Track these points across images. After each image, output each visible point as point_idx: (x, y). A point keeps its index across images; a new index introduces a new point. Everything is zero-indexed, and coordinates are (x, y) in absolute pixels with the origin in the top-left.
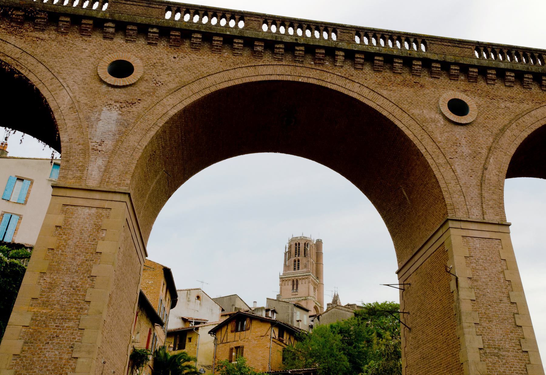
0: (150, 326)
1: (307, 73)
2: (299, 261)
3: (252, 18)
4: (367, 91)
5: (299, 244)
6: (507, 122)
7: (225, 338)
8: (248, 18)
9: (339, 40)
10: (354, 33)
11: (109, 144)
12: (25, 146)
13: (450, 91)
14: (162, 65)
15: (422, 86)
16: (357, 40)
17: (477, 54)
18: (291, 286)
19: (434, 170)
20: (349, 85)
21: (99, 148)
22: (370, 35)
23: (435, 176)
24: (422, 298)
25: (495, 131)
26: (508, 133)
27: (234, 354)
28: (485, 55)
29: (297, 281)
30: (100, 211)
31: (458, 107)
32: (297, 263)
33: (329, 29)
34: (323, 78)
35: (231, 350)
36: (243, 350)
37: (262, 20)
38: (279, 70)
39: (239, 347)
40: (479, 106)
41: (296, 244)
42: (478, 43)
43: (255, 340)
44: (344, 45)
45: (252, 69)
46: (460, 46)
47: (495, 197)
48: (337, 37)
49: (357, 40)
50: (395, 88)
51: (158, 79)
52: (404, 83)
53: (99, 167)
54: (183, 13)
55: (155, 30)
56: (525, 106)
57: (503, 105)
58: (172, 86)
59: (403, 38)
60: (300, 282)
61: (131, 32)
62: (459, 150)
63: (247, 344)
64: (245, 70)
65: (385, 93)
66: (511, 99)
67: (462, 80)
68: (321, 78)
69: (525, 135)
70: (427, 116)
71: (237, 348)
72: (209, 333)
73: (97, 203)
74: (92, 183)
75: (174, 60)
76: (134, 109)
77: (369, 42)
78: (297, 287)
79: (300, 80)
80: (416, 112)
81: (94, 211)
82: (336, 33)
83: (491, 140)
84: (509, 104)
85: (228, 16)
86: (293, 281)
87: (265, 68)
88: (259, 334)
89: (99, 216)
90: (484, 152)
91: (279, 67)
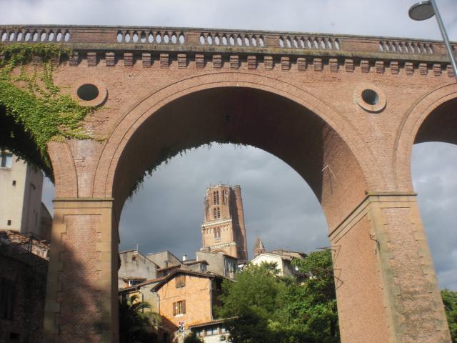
0: (145, 301)
1: (243, 78)
2: (219, 209)
3: (190, 33)
4: (295, 89)
5: (218, 192)
6: (409, 106)
7: (167, 295)
8: (187, 33)
9: (267, 45)
10: (278, 37)
11: (89, 159)
12: (18, 168)
13: (362, 81)
14: (121, 84)
15: (340, 80)
16: (281, 43)
17: (381, 47)
18: (214, 234)
19: (355, 154)
20: (279, 86)
21: (83, 164)
22: (292, 38)
23: (356, 159)
24: (352, 257)
25: (401, 115)
26: (411, 116)
27: (177, 308)
28: (388, 48)
29: (218, 228)
30: (93, 217)
31: (369, 97)
32: (217, 211)
33: (257, 36)
34: (256, 81)
35: (174, 304)
36: (185, 304)
37: (199, 34)
38: (220, 78)
39: (181, 301)
40: (386, 94)
41: (215, 193)
42: (381, 38)
43: (195, 294)
44: (270, 50)
45: (196, 79)
46: (367, 41)
47: (404, 172)
48: (264, 43)
49: (281, 43)
50: (317, 84)
51: (120, 97)
52: (325, 79)
53: (85, 180)
54: (132, 35)
55: (111, 54)
56: (424, 91)
57: (405, 91)
58: (133, 102)
59: (320, 39)
60: (222, 229)
61: (91, 58)
62: (373, 135)
63: (188, 298)
64: (190, 80)
65: (309, 89)
66: (412, 86)
67: (373, 72)
68: (254, 81)
69: (424, 116)
70: (346, 108)
71: (179, 302)
72: (152, 291)
73: (90, 211)
74: (84, 193)
75: (129, 78)
76: (104, 126)
77: (291, 45)
78: (219, 235)
79: (238, 85)
80: (337, 104)
81: (88, 217)
82: (263, 39)
83: (399, 124)
84: (410, 90)
85: (170, 33)
86: (215, 228)
87: (206, 77)
88: (199, 288)
89: (93, 222)
90: (394, 134)
91: (219, 75)
